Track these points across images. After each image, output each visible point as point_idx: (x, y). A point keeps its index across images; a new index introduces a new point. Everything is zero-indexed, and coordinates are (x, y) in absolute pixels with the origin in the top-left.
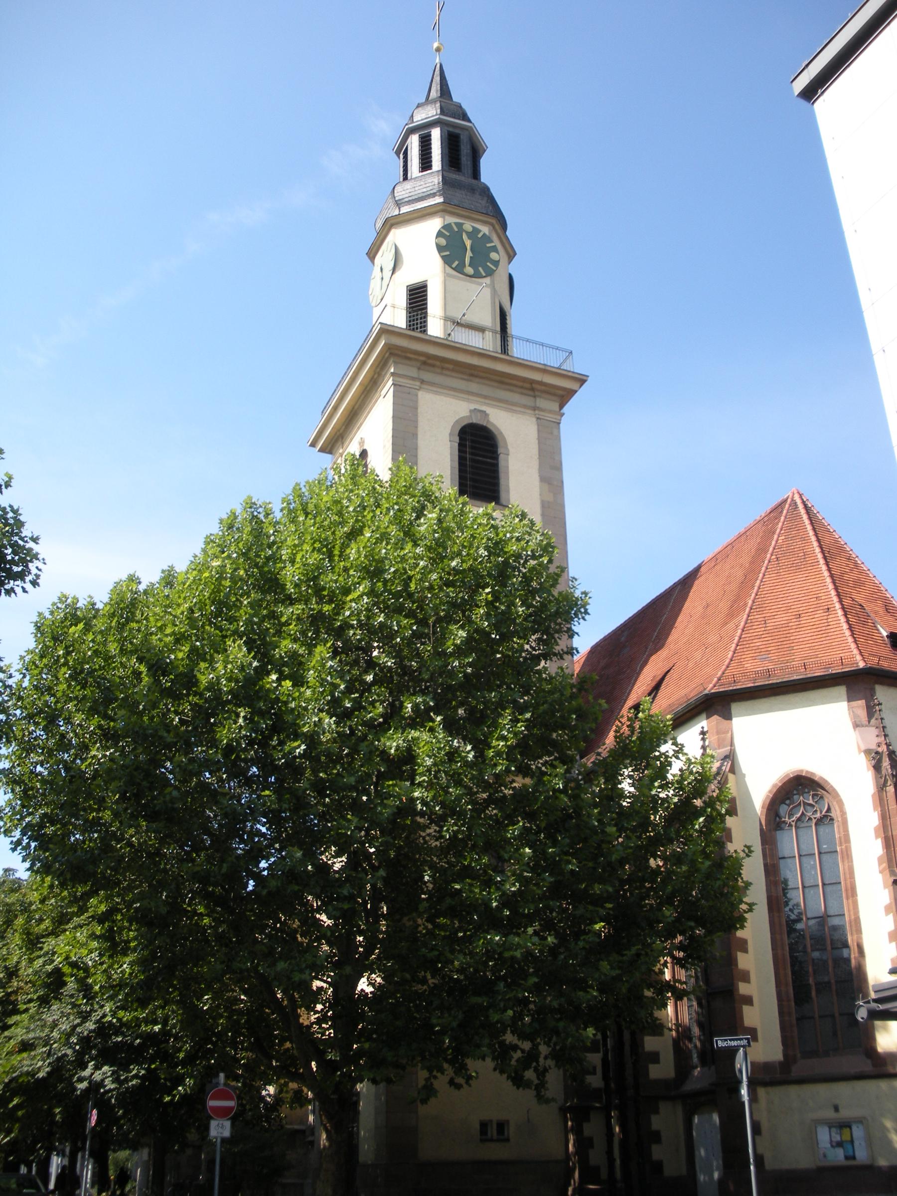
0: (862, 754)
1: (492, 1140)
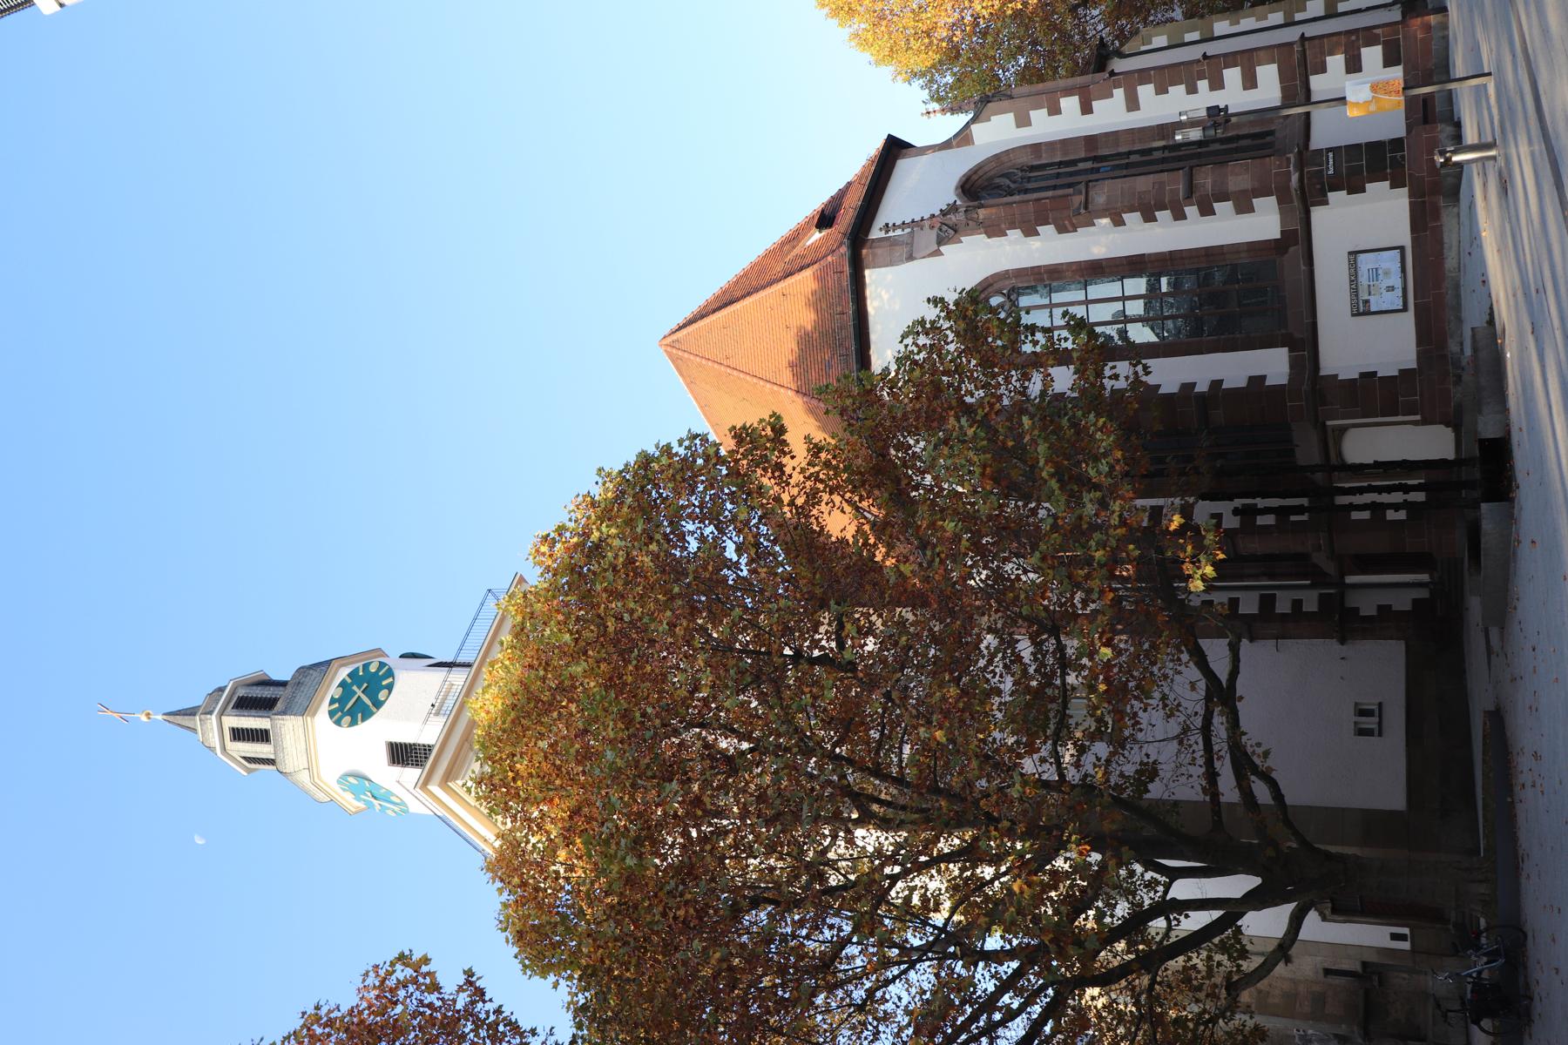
0: (942, 249)
1: (1380, 724)
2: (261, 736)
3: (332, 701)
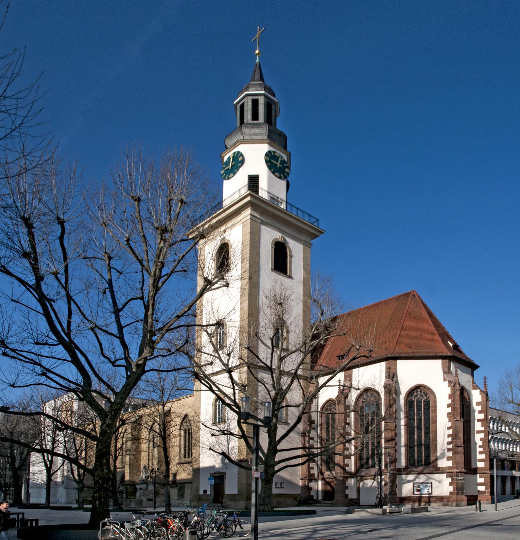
0: (447, 382)
2: (255, 116)
3: (274, 152)
